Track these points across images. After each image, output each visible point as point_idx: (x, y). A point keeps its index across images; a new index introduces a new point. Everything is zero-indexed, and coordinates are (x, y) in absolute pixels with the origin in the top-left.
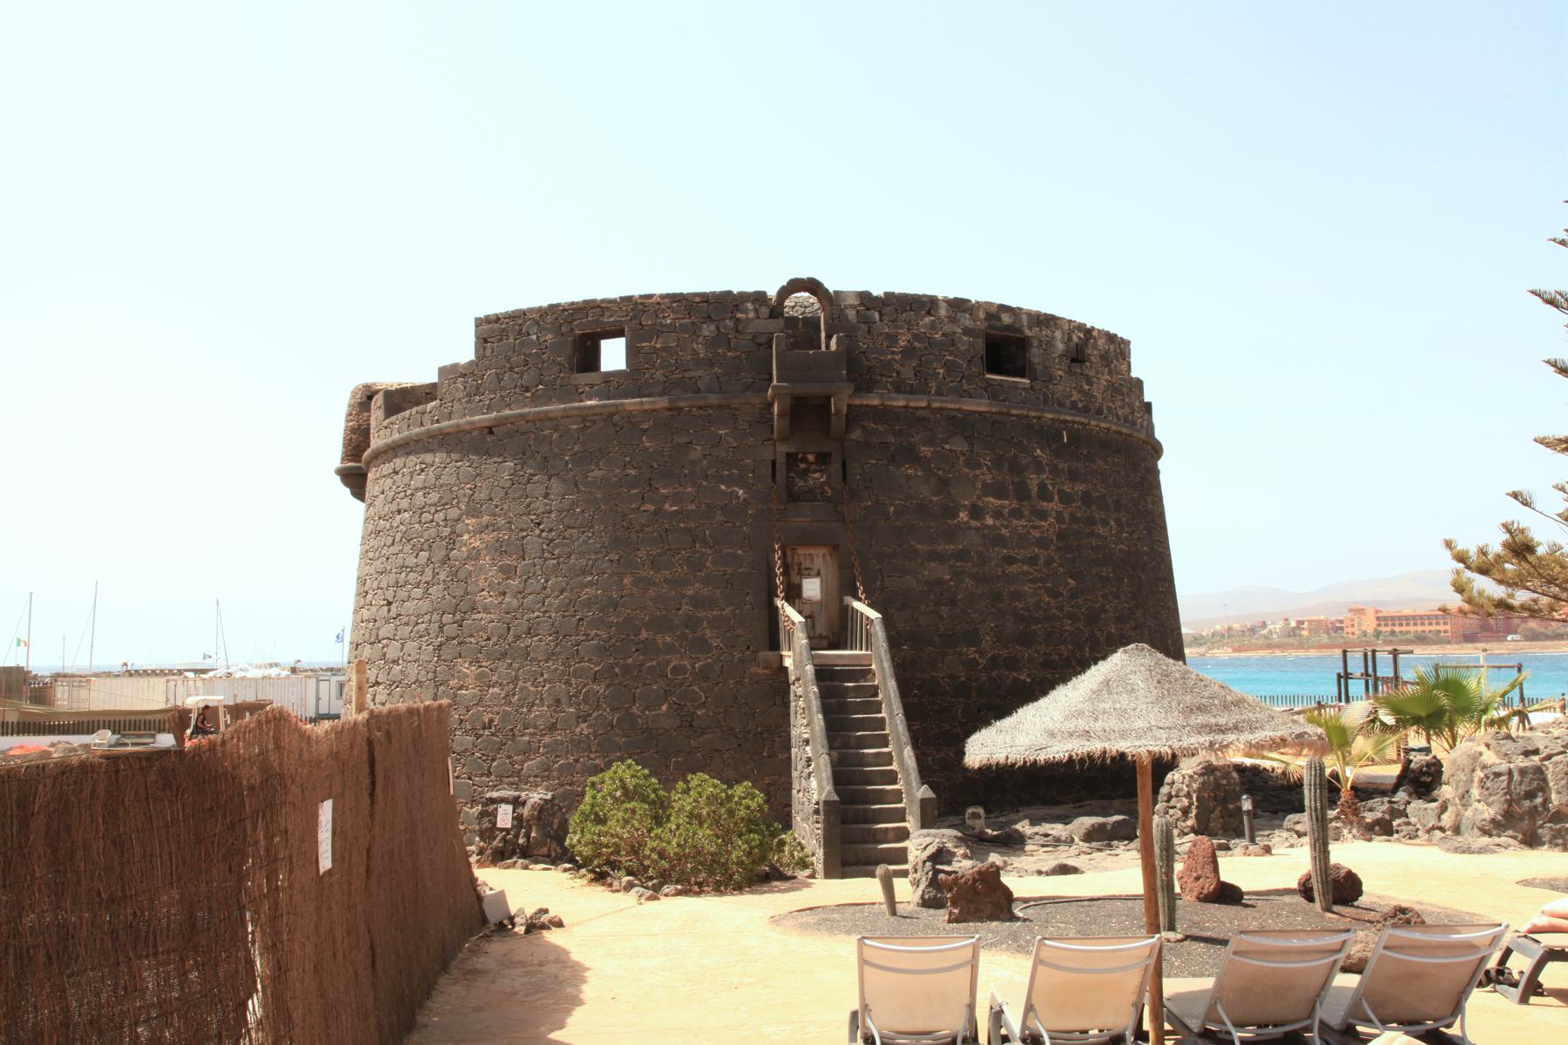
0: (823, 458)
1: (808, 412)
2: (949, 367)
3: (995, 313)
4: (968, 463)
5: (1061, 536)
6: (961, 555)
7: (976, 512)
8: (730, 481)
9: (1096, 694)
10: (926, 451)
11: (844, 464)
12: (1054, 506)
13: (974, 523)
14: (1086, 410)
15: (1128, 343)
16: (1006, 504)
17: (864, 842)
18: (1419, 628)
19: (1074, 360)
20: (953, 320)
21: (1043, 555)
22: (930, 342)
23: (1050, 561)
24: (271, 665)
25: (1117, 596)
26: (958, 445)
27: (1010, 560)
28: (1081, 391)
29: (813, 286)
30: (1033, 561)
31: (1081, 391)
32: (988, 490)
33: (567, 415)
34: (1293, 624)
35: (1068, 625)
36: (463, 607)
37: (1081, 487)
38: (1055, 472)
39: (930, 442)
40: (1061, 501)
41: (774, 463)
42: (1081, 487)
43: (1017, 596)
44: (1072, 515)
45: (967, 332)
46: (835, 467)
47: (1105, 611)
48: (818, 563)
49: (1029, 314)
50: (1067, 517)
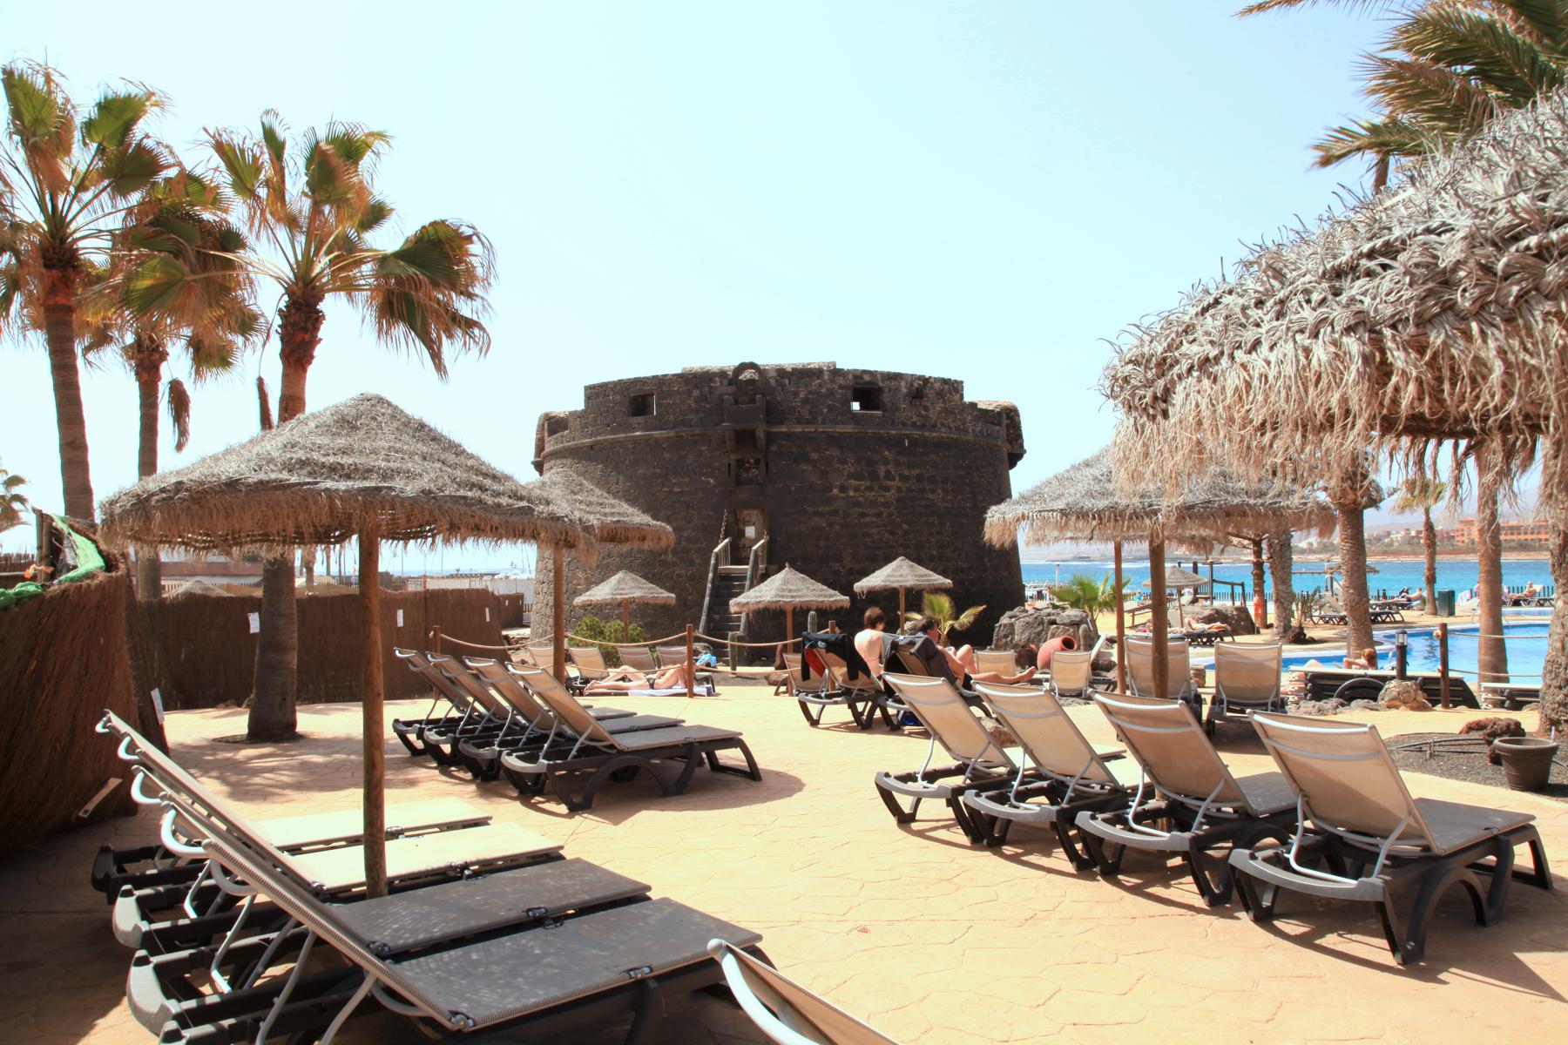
0: (757, 461)
1: (744, 438)
2: (831, 408)
4: (840, 462)
5: (898, 500)
6: (834, 513)
7: (843, 489)
8: (707, 475)
9: (619, 582)
10: (814, 456)
12: (896, 483)
14: (923, 426)
16: (863, 484)
18: (1522, 537)
20: (832, 381)
21: (886, 512)
22: (819, 393)
23: (890, 515)
24: (452, 577)
26: (834, 452)
27: (864, 515)
28: (920, 415)
29: (752, 366)
30: (879, 515)
31: (920, 415)
32: (851, 476)
33: (626, 440)
34: (1413, 533)
37: (916, 472)
38: (897, 463)
42: (916, 472)
43: (867, 535)
45: (841, 387)
46: (763, 465)
48: (754, 518)
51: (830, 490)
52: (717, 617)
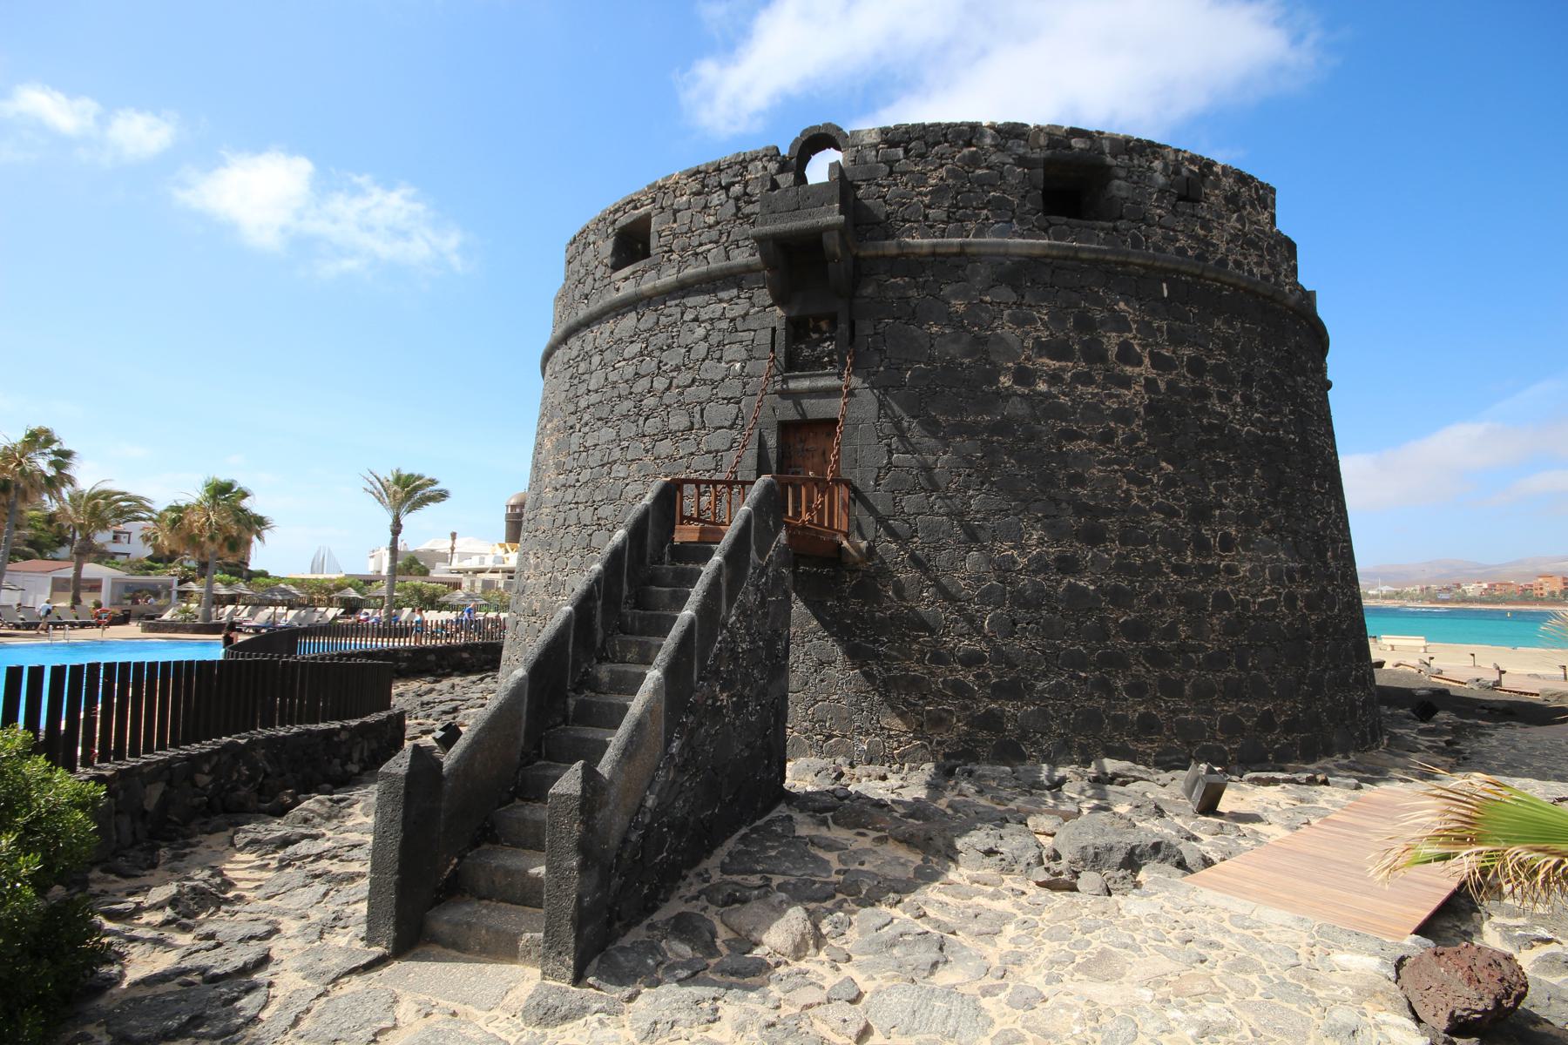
3: (1059, 140)
6: (1003, 427)
7: (1024, 376)
11: (852, 326)
12: (1146, 369)
15: (1273, 191)
16: (1070, 368)
19: (1180, 198)
23: (1132, 439)
25: (1242, 489)
27: (1072, 436)
28: (1195, 238)
30: (1108, 437)
32: (1042, 348)
35: (1158, 520)
37: (1187, 352)
40: (1153, 366)
42: (1187, 352)
45: (1021, 161)
47: (1221, 506)
49: (1114, 140)
50: (1162, 386)
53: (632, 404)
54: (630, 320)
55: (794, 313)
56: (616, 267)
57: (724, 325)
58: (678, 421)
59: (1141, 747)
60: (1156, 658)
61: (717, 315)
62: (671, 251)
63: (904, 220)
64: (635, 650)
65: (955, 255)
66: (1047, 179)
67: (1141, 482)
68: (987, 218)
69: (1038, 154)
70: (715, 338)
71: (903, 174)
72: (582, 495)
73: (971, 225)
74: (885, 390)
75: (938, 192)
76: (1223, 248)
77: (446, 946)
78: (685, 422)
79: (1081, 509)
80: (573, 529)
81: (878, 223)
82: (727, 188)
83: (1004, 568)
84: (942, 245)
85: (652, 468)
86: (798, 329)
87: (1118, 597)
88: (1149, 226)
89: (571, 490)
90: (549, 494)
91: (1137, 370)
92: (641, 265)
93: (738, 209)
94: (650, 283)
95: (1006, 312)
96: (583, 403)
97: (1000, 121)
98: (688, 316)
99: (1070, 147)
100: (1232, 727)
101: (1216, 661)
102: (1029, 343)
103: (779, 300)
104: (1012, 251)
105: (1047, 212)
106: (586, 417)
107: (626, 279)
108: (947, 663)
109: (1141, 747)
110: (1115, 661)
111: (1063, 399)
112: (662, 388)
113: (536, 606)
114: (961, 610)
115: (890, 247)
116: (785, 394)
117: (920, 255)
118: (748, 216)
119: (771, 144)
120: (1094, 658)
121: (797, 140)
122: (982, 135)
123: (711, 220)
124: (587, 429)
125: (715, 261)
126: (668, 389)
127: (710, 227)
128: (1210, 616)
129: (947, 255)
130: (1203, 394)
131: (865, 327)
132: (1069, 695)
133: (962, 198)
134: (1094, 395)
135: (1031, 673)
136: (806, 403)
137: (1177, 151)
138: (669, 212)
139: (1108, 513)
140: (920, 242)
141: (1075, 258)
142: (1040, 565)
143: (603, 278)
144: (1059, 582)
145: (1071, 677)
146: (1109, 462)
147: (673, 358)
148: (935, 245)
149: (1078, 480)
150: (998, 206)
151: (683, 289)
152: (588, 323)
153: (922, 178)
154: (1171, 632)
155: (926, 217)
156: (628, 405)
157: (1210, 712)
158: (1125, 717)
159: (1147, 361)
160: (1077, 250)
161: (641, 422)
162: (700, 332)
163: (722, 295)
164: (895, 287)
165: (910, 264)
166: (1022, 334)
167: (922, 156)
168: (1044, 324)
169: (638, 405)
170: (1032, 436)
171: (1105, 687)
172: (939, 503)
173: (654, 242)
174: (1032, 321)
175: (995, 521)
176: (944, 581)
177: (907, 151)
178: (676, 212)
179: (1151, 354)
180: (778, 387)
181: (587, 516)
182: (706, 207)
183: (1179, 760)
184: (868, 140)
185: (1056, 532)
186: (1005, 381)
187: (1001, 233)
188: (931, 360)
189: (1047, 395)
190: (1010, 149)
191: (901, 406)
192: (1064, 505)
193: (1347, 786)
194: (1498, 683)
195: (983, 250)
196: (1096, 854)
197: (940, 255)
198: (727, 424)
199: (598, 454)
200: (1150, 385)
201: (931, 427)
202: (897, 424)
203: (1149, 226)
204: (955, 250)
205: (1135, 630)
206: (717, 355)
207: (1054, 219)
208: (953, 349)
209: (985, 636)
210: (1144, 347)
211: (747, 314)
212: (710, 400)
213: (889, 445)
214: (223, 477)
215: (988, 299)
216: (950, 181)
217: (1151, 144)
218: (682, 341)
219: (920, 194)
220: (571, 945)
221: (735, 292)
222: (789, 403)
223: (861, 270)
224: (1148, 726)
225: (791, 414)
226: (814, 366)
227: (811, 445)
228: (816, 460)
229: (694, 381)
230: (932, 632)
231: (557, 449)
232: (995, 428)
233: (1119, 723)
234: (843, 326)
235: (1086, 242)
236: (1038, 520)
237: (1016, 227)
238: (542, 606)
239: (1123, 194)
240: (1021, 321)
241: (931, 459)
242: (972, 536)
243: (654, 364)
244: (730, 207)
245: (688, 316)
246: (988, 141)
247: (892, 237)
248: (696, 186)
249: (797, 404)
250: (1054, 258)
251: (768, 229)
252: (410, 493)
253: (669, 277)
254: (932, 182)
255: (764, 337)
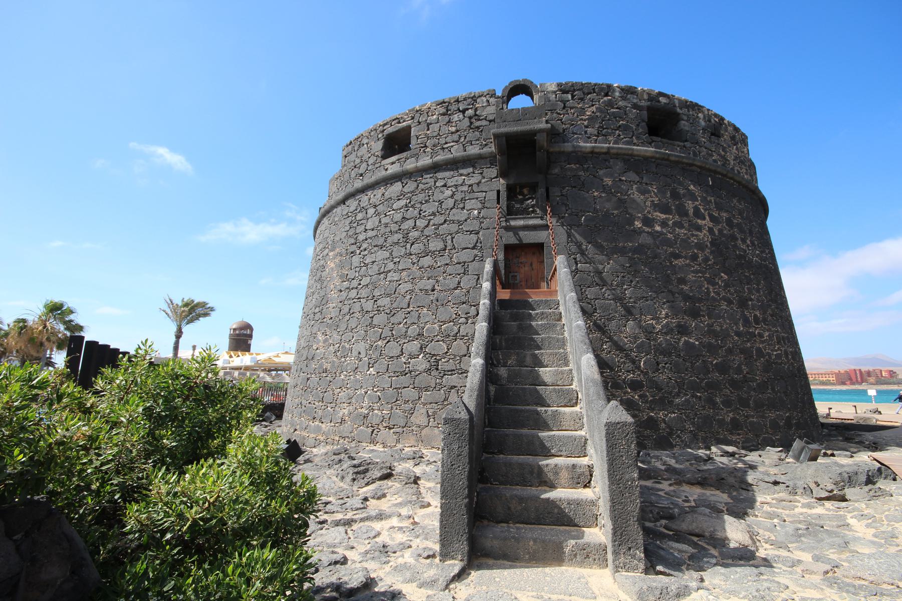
3: (654, 97)
7: (647, 222)
12: (706, 222)
13: (647, 229)
16: (672, 219)
17: (524, 483)
19: (712, 134)
23: (706, 260)
27: (677, 256)
28: (720, 155)
32: (655, 206)
35: (724, 306)
36: (324, 301)
39: (610, 175)
41: (498, 192)
44: (720, 231)
45: (635, 106)
47: (751, 300)
49: (680, 100)
51: (631, 222)
52: (503, 372)
53: (401, 236)
54: (397, 187)
55: (511, 182)
56: (384, 157)
57: (465, 188)
58: (435, 245)
59: (734, 438)
60: (734, 384)
61: (460, 182)
62: (426, 146)
63: (574, 133)
64: (514, 357)
65: (605, 153)
66: (649, 118)
67: (714, 284)
68: (619, 135)
69: (643, 103)
70: (458, 196)
71: (571, 108)
72: (364, 293)
73: (611, 138)
74: (571, 226)
75: (592, 119)
76: (732, 163)
77: (497, 557)
78: (440, 245)
79: (686, 298)
80: (357, 315)
81: (558, 134)
82: (464, 112)
83: (649, 332)
84: (598, 147)
85: (418, 274)
86: (512, 191)
87: (712, 349)
88: (700, 147)
89: (355, 291)
90: (334, 295)
91: (704, 222)
92: (404, 155)
93: (471, 123)
94: (410, 165)
95: (635, 186)
96: (361, 237)
97: (623, 85)
98: (439, 184)
99: (659, 101)
100: (775, 425)
101: (762, 387)
102: (648, 203)
103: (503, 174)
104: (635, 153)
105: (650, 135)
106: (365, 246)
107: (393, 163)
108: (621, 388)
109: (734, 438)
110: (713, 386)
111: (669, 236)
112: (423, 225)
113: (329, 366)
114: (627, 356)
115: (568, 147)
116: (508, 228)
117: (584, 153)
118: (478, 127)
119: (492, 88)
120: (703, 384)
121: (506, 87)
122: (614, 91)
123: (454, 129)
124: (366, 252)
125: (456, 152)
126: (427, 226)
127: (452, 133)
128: (756, 360)
129: (600, 154)
130: (733, 238)
131: (555, 192)
132: (693, 407)
133: (606, 123)
134: (685, 234)
135: (671, 393)
136: (521, 233)
137: (708, 110)
138: (424, 125)
139: (700, 300)
140: (587, 146)
141: (668, 160)
142: (668, 330)
143: (374, 164)
144: (679, 340)
145: (692, 396)
146: (696, 272)
147: (429, 208)
148: (594, 147)
149: (682, 281)
150: (625, 128)
151: (435, 168)
152: (363, 190)
153: (582, 111)
154: (739, 370)
155: (586, 132)
156: (396, 237)
157: (763, 417)
158: (724, 420)
159: (707, 217)
160: (669, 155)
161: (408, 246)
162: (448, 193)
163: (461, 171)
164: (571, 169)
165: (581, 158)
166: (644, 198)
167: (582, 99)
168: (655, 194)
169: (406, 236)
170: (656, 256)
171: (711, 402)
172: (608, 292)
173: (413, 141)
174: (649, 192)
175: (640, 304)
176: (615, 338)
177: (573, 97)
178: (428, 125)
179: (709, 214)
180: (504, 224)
181: (369, 305)
182: (449, 122)
183: (753, 446)
184: (550, 89)
185: (675, 311)
186: (638, 224)
187: (628, 143)
188: (595, 211)
189: (661, 233)
190: (629, 99)
191: (581, 235)
192: (677, 295)
193: (846, 456)
194: (829, 415)
195: (620, 151)
196: (850, 477)
197: (597, 153)
198: (471, 246)
199: (375, 267)
200: (711, 230)
201: (599, 247)
202: (579, 246)
203: (700, 147)
204: (604, 150)
205: (722, 368)
206: (461, 206)
207: (655, 138)
208: (608, 205)
209: (642, 372)
210: (705, 210)
211: (480, 182)
212: (457, 232)
213: (575, 259)
214: (57, 299)
215: (624, 178)
216: (598, 114)
217: (697, 105)
218: (435, 198)
219: (582, 119)
220: (641, 541)
221: (471, 170)
222: (511, 234)
223: (552, 159)
224: (735, 426)
225: (513, 240)
226: (525, 212)
227: (523, 260)
228: (526, 269)
229: (445, 221)
230: (612, 369)
231: (341, 266)
232: (635, 250)
233: (721, 423)
234: (541, 191)
235: (673, 152)
236: (664, 304)
237: (635, 141)
238: (333, 365)
239: (687, 128)
240: (643, 192)
241: (601, 267)
242: (629, 312)
243: (416, 212)
244: (466, 122)
245: (439, 184)
246: (617, 94)
247: (568, 142)
248: (443, 110)
249: (516, 234)
250: (657, 159)
251: (503, 130)
252: (193, 312)
253: (425, 161)
254: (588, 113)
255: (493, 195)
